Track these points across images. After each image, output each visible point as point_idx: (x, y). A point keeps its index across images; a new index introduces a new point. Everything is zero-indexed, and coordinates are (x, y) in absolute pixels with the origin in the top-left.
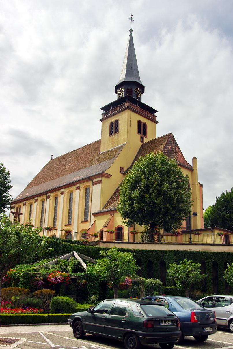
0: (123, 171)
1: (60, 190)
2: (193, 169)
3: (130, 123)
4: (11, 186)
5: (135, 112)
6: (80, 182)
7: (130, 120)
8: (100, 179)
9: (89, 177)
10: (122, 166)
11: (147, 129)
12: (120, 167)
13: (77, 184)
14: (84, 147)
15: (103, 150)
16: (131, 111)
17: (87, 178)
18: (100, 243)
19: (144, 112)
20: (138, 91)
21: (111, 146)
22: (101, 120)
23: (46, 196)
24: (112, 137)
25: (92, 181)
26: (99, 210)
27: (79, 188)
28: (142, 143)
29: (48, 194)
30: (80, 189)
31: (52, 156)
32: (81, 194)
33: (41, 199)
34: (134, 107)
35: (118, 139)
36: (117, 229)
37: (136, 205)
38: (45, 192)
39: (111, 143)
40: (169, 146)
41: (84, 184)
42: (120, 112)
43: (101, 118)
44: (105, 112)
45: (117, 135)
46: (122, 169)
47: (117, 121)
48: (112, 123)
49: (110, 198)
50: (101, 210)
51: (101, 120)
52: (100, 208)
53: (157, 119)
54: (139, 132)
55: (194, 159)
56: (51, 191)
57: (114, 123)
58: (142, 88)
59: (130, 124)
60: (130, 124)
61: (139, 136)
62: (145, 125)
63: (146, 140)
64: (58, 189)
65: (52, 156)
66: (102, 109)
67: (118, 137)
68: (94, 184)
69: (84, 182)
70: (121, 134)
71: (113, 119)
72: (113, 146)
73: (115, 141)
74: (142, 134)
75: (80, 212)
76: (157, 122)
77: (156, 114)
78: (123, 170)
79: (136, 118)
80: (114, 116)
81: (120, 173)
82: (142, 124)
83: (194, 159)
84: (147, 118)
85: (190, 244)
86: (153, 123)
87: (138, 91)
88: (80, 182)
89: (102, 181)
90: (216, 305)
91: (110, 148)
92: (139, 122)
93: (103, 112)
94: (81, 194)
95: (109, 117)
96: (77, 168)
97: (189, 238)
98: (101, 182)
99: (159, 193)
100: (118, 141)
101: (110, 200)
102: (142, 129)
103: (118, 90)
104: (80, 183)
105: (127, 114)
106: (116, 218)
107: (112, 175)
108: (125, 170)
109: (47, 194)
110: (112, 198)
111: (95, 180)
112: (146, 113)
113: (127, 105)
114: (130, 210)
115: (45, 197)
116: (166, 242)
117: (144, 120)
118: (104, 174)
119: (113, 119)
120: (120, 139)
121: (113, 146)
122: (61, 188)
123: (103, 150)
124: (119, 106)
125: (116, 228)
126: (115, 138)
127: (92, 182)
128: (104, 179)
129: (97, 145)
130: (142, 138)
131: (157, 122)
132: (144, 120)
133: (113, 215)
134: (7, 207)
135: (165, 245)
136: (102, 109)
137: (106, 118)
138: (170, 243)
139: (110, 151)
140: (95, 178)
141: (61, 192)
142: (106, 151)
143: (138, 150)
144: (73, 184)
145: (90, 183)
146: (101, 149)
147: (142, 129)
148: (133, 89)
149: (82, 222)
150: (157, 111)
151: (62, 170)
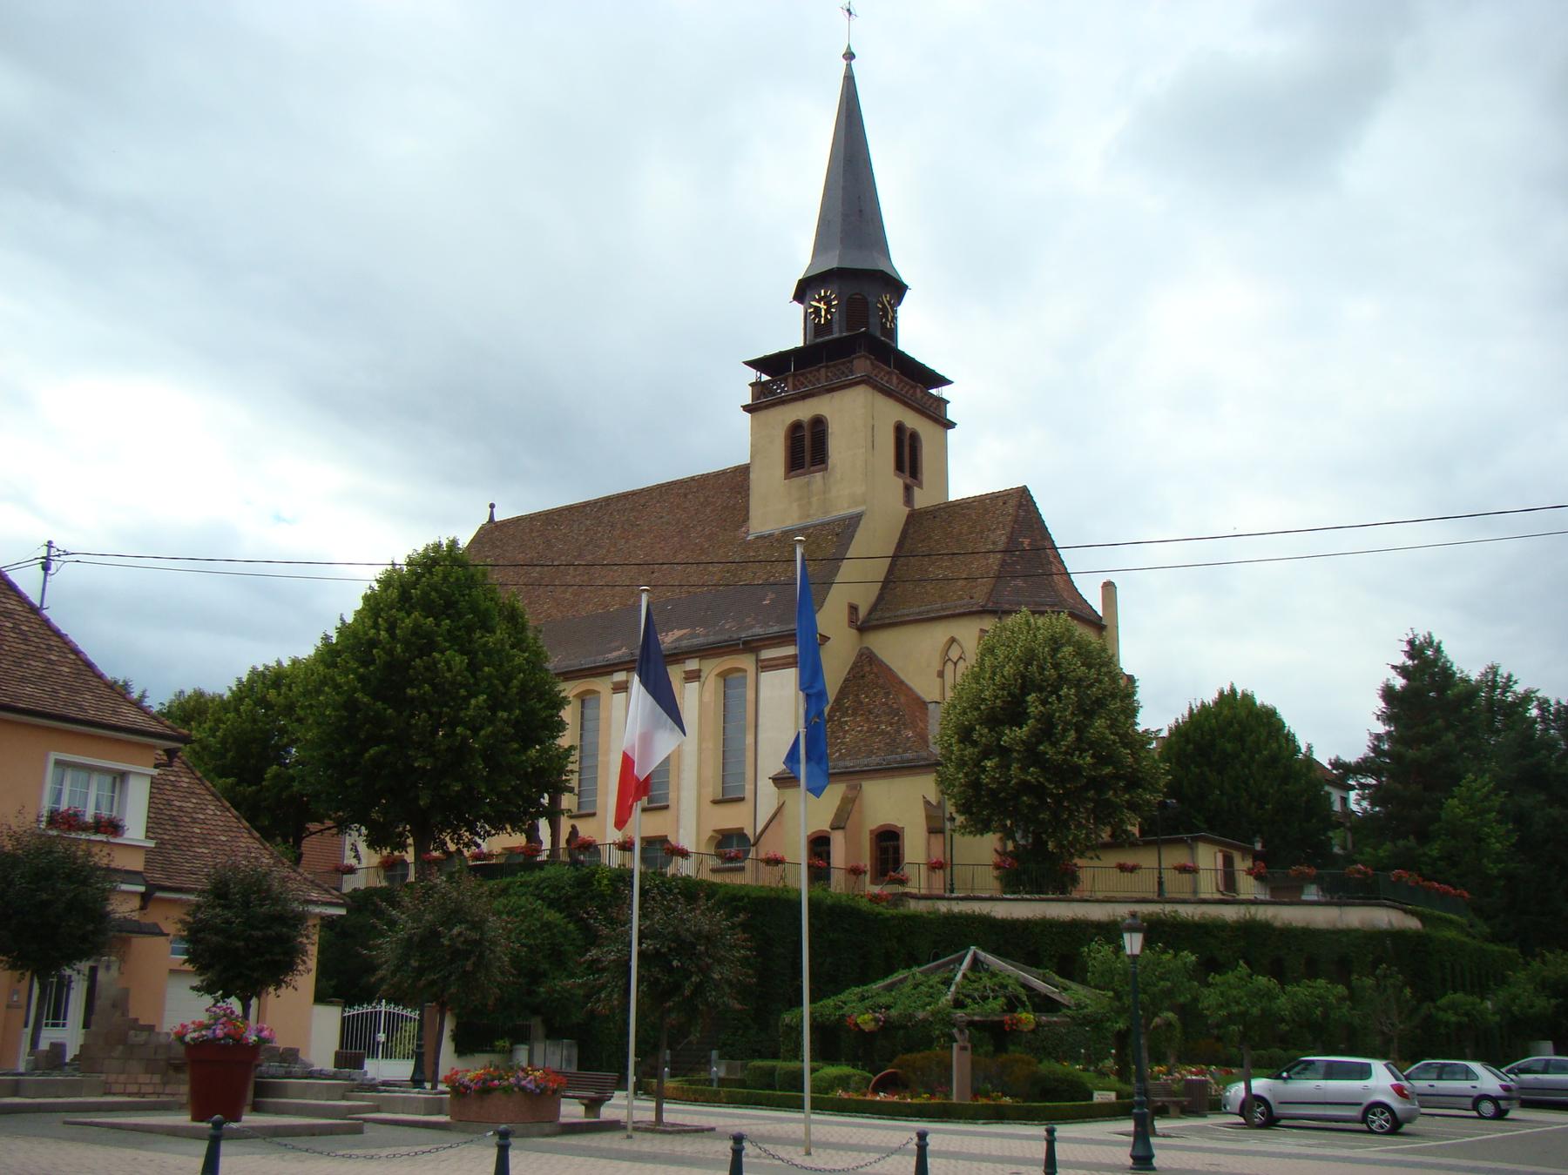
0: (857, 619)
1: (611, 673)
2: (1104, 622)
3: (873, 436)
4: (339, 626)
5: (888, 393)
6: (701, 654)
7: (873, 426)
10: (855, 602)
11: (922, 454)
12: (849, 603)
13: (688, 658)
16: (875, 392)
18: (910, 900)
19: (912, 387)
20: (889, 307)
22: (747, 408)
25: (757, 656)
27: (700, 677)
28: (907, 510)
30: (702, 679)
31: (492, 506)
32: (708, 697)
36: (877, 836)
40: (1025, 537)
43: (749, 401)
44: (765, 378)
46: (853, 609)
48: (796, 427)
51: (747, 408)
53: (951, 413)
54: (899, 467)
55: (1109, 588)
57: (806, 426)
59: (873, 442)
60: (873, 442)
61: (898, 483)
62: (914, 437)
63: (922, 499)
65: (492, 506)
66: (754, 364)
67: (825, 484)
71: (803, 411)
73: (814, 499)
74: (908, 474)
76: (951, 425)
79: (892, 413)
80: (806, 401)
81: (850, 626)
82: (908, 434)
83: (1109, 588)
86: (939, 429)
87: (889, 307)
88: (701, 654)
90: (860, 1063)
92: (899, 429)
93: (752, 375)
97: (1156, 880)
99: (1081, 744)
104: (702, 658)
107: (829, 638)
111: (767, 654)
112: (918, 390)
116: (1100, 895)
119: (803, 411)
122: (617, 668)
125: (872, 832)
127: (757, 661)
130: (908, 490)
131: (951, 425)
132: (913, 421)
135: (1096, 904)
136: (754, 364)
141: (615, 684)
143: (898, 535)
145: (746, 662)
148: (869, 299)
149: (715, 802)
150: (948, 382)
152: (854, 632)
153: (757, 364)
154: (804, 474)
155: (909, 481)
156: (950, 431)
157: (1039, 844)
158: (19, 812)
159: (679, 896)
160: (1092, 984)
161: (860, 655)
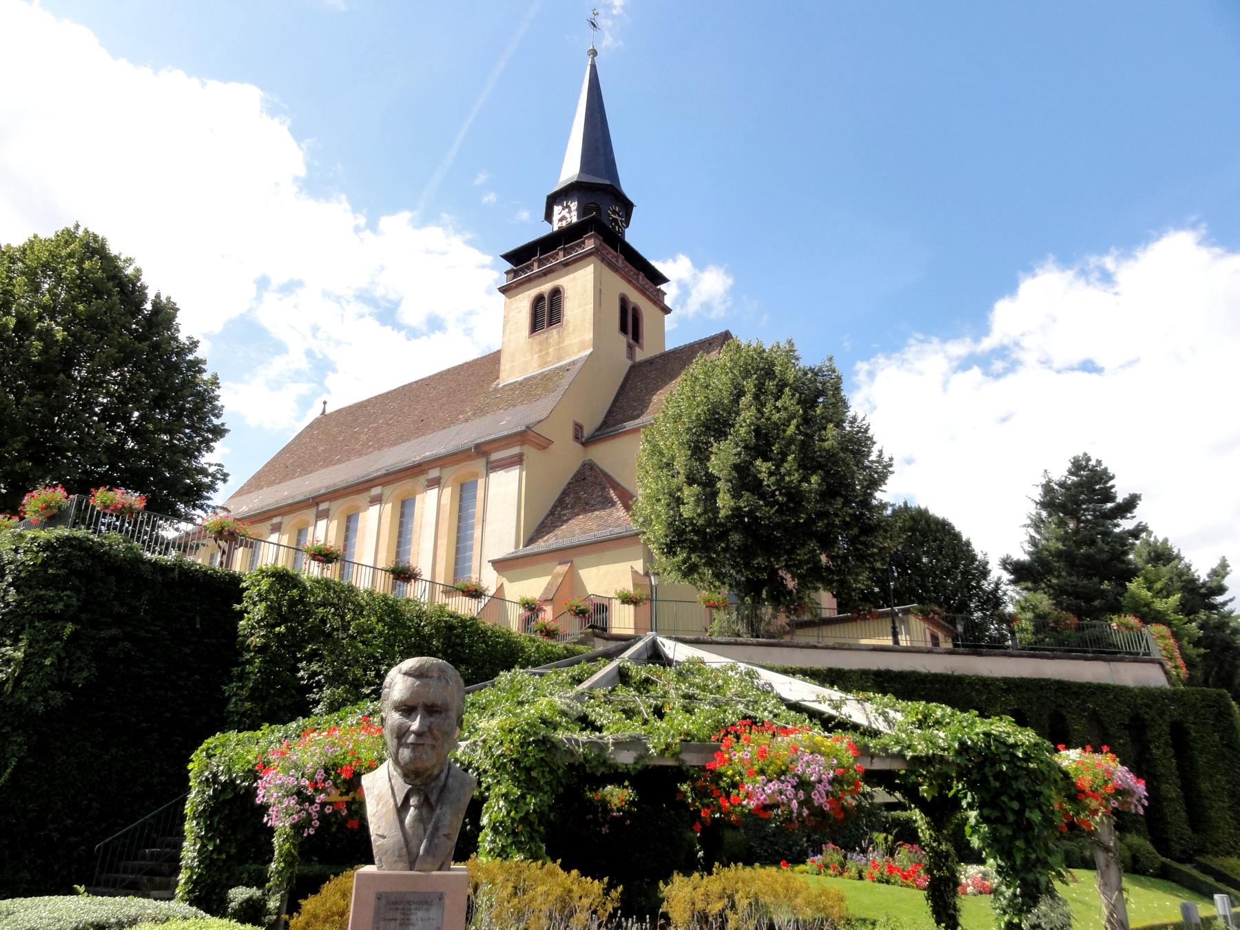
0: (582, 437)
1: (369, 489)
8: (515, 450)
9: (477, 446)
10: (579, 421)
14: (436, 375)
15: (510, 374)
17: (471, 449)
18: (595, 639)
21: (535, 365)
22: (504, 290)
23: (314, 510)
24: (541, 336)
26: (513, 550)
28: (630, 363)
29: (323, 506)
31: (325, 403)
33: (295, 521)
34: (611, 253)
35: (559, 343)
37: (724, 502)
38: (314, 498)
39: (536, 356)
41: (456, 467)
42: (566, 264)
45: (559, 332)
46: (578, 428)
47: (556, 293)
48: (539, 299)
49: (548, 516)
50: (522, 550)
51: (504, 290)
52: (517, 545)
54: (623, 329)
56: (334, 494)
57: (546, 297)
58: (627, 207)
61: (622, 341)
63: (641, 355)
64: (361, 487)
65: (325, 403)
67: (560, 337)
68: (493, 467)
69: (457, 462)
70: (571, 329)
71: (545, 288)
72: (545, 364)
74: (631, 336)
75: (438, 560)
77: (663, 287)
78: (582, 432)
79: (619, 286)
84: (643, 291)
85: (896, 649)
89: (525, 458)
91: (534, 369)
92: (624, 301)
93: (509, 266)
94: (443, 502)
95: (529, 280)
96: (422, 427)
98: (518, 460)
100: (559, 349)
101: (546, 518)
102: (630, 322)
103: (557, 209)
104: (442, 467)
105: (591, 268)
106: (581, 572)
108: (587, 432)
109: (317, 504)
110: (552, 513)
111: (495, 456)
113: (590, 244)
114: (699, 515)
115: (310, 513)
117: (635, 298)
118: (532, 434)
120: (566, 343)
121: (541, 366)
123: (510, 374)
124: (565, 249)
126: (551, 341)
128: (530, 452)
129: (491, 362)
130: (630, 347)
131: (667, 310)
132: (635, 298)
133: (572, 562)
134: (202, 505)
137: (520, 284)
138: (845, 644)
139: (534, 377)
140: (497, 450)
142: (519, 379)
144: (415, 470)
146: (503, 375)
147: (630, 322)
151: (364, 437)
152: (581, 446)
153: (508, 257)
154: (544, 333)
155: (631, 341)
156: (667, 317)
157: (827, 472)
158: (888, 882)
159: (643, 805)
160: (342, 903)
161: (584, 465)
